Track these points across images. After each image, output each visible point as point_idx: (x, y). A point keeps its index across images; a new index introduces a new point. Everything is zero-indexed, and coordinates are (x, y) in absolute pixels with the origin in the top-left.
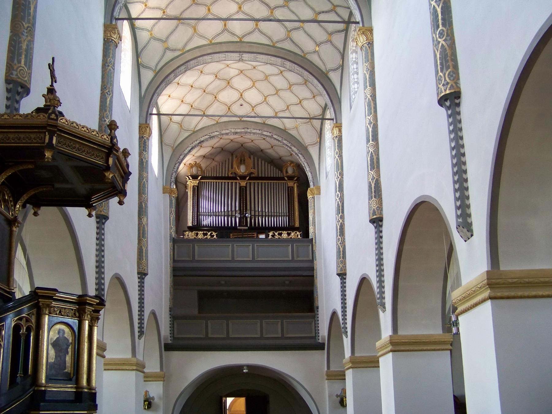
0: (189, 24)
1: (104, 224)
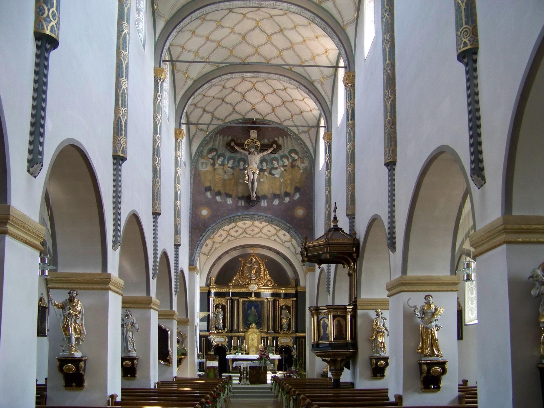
0: (200, 58)
1: (120, 165)
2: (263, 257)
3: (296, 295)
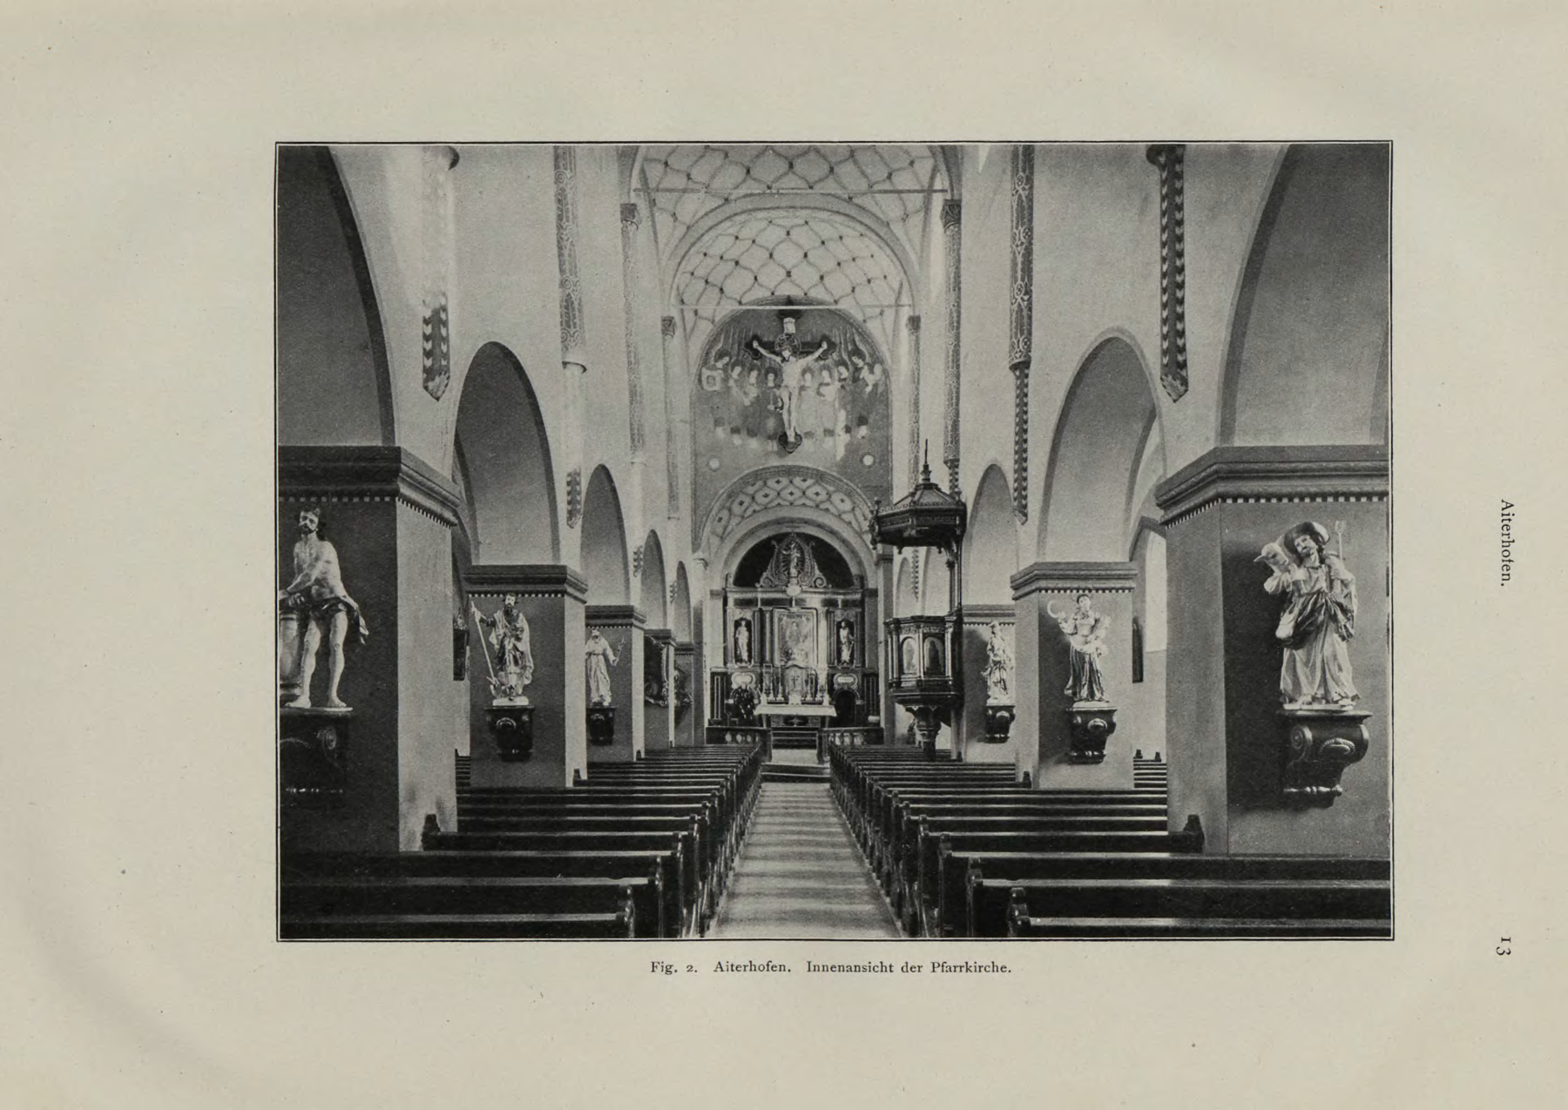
2: (808, 538)
3: (861, 603)
